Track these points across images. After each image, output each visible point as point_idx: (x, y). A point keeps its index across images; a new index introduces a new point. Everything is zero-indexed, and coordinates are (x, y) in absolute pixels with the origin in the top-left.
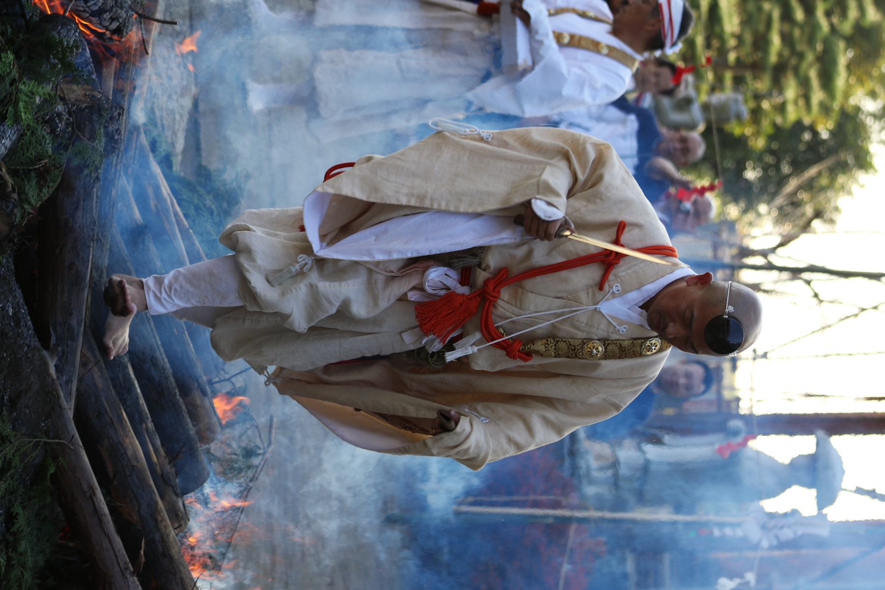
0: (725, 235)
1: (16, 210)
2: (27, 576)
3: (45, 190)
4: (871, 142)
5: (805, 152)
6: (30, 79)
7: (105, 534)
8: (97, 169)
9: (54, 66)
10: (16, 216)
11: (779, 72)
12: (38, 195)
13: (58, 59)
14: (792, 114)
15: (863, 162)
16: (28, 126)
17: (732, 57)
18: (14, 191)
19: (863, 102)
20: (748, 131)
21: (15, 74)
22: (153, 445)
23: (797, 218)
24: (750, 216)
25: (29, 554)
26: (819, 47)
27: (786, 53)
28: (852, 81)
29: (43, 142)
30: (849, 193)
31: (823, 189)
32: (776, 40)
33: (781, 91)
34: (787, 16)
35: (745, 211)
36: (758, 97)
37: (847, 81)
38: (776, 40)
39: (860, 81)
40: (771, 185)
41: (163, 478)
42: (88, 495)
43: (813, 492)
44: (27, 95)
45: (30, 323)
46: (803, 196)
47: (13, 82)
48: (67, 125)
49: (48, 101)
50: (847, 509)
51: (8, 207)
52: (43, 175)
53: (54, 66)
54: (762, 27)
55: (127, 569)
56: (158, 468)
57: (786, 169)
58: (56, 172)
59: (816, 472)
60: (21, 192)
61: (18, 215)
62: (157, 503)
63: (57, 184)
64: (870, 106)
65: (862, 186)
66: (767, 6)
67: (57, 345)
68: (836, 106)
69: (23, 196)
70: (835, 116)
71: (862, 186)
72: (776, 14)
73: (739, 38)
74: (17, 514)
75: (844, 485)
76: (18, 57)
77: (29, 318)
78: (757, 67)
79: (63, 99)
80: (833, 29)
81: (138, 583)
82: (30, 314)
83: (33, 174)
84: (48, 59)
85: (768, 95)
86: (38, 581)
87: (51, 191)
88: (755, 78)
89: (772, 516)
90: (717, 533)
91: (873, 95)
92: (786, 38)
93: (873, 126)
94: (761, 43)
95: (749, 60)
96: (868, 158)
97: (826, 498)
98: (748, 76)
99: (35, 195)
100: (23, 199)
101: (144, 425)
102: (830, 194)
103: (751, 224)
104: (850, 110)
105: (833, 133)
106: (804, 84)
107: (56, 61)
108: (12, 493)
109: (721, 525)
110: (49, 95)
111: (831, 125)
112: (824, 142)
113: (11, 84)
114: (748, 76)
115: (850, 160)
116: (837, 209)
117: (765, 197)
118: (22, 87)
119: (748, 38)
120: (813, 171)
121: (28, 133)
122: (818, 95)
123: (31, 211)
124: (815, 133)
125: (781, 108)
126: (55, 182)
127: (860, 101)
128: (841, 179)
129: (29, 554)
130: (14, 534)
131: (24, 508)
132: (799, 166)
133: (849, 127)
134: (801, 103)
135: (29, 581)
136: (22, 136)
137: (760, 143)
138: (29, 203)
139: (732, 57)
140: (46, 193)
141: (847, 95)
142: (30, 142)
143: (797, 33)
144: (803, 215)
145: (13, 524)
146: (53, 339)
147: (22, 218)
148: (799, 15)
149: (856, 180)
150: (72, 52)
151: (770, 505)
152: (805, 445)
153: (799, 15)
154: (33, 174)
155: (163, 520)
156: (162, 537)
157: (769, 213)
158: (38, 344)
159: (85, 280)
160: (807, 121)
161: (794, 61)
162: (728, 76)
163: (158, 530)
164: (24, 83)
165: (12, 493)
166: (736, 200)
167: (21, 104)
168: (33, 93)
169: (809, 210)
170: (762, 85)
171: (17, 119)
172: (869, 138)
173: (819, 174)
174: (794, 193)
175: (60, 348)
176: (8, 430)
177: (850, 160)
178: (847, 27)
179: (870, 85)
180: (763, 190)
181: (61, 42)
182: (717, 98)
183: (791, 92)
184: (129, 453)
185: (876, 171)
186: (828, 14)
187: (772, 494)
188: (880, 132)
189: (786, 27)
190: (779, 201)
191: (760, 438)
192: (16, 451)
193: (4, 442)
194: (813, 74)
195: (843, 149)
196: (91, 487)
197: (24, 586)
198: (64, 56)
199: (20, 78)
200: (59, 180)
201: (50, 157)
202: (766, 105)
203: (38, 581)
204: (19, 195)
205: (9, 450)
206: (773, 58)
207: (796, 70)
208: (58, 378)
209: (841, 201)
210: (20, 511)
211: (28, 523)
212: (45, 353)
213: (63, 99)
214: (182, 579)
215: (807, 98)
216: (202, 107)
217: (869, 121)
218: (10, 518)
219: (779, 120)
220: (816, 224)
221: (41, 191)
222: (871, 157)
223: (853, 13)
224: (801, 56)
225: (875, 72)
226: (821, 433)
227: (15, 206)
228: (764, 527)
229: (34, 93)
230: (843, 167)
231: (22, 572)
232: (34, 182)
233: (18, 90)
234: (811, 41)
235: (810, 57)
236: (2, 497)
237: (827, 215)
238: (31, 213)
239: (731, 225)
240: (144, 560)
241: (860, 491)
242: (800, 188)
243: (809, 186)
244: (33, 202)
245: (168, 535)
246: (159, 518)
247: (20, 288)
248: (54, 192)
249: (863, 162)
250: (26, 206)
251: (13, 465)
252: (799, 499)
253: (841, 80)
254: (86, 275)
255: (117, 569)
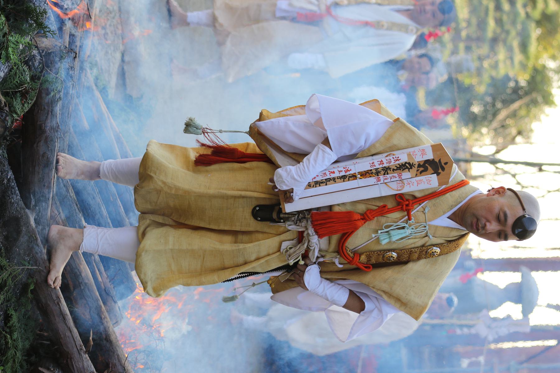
0: (461, 146)
1: (7, 118)
2: (19, 354)
3: (26, 105)
4: (553, 88)
5: (510, 94)
6: (16, 33)
7: (67, 327)
8: (60, 92)
9: (31, 25)
10: (7, 121)
11: (495, 40)
12: (22, 108)
13: (34, 21)
14: (502, 71)
15: (548, 100)
16: (15, 63)
17: (464, 34)
18: (6, 106)
19: (547, 62)
20: (474, 81)
21: (6, 29)
22: (99, 270)
23: (505, 136)
24: (476, 135)
25: (20, 340)
26: (519, 27)
27: (498, 31)
28: (541, 48)
29: (24, 73)
30: (539, 120)
31: (522, 117)
32: (491, 24)
33: (496, 54)
34: (498, 8)
35: (473, 131)
36: (480, 59)
37: (537, 49)
38: (491, 24)
39: (545, 49)
40: (488, 116)
41: (105, 291)
42: (56, 302)
43: (520, 306)
44: (14, 44)
45: (18, 192)
46: (510, 122)
47: (5, 35)
48: (40, 63)
49: (29, 46)
50: (541, 317)
51: (2, 116)
52: (24, 95)
53: (31, 25)
54: (482, 14)
55: (81, 349)
56: (102, 285)
57: (499, 105)
58: (33, 93)
59: (522, 294)
60: (11, 106)
61: (10, 121)
62: (101, 307)
63: (33, 102)
64: (552, 64)
65: (547, 116)
66: (485, 2)
67: (35, 206)
68: (530, 64)
69: (12, 109)
70: (530, 70)
71: (547, 116)
72: (492, 6)
73: (469, 22)
74: (12, 314)
75: (539, 302)
76: (8, 19)
77: (17, 188)
78: (479, 39)
79: (37, 47)
80: (528, 16)
81: (88, 358)
82: (18, 186)
83: (18, 94)
84: (27, 21)
85: (488, 57)
86: (26, 358)
87: (30, 106)
88: (478, 47)
89: (495, 319)
90: (459, 332)
91: (554, 58)
92: (499, 22)
93: (554, 77)
94: (482, 25)
95: (474, 36)
96: (551, 98)
97: (526, 311)
98: (474, 45)
99: (21, 108)
100: (12, 111)
101: (93, 257)
102: (526, 120)
103: (477, 140)
104: (539, 68)
105: (529, 83)
106: (510, 49)
107: (33, 22)
108: (8, 301)
109: (461, 326)
110: (28, 43)
111: (527, 76)
112: (522, 88)
113: (4, 36)
114: (474, 45)
115: (540, 99)
116: (531, 131)
117: (486, 123)
118: (10, 38)
119: (474, 21)
120: (516, 105)
121: (15, 68)
122: (518, 57)
123: (18, 118)
124: (517, 82)
125: (495, 66)
126: (32, 100)
127: (545, 61)
128: (534, 110)
129: (20, 340)
130: (10, 328)
131: (16, 311)
132: (507, 103)
133: (539, 78)
134: (508, 62)
135: (20, 358)
136: (10, 71)
137: (482, 89)
138: (16, 113)
139: (464, 34)
140: (27, 107)
141: (537, 58)
142: (16, 73)
143: (505, 18)
144: (510, 134)
145: (9, 321)
146: (33, 203)
147: (12, 123)
148: (506, 7)
149: (544, 112)
150: (42, 16)
151: (493, 314)
152: (515, 277)
153: (506, 7)
154: (18, 94)
155: (105, 318)
156: (105, 328)
157: (488, 133)
158: (23, 205)
159: (53, 163)
160: (511, 74)
161: (503, 36)
162: (462, 46)
163: (103, 324)
164: (12, 36)
165: (8, 301)
166: (466, 125)
167: (10, 49)
168: (18, 43)
169: (514, 131)
170: (484, 50)
171: (8, 58)
172: (551, 85)
173: (520, 107)
174: (505, 120)
175: (37, 208)
176: (4, 262)
177: (540, 99)
178: (536, 14)
179: (551, 51)
180: (484, 118)
181: (35, 9)
182: (454, 59)
183: (502, 55)
184: (83, 275)
185: (556, 106)
186: (525, 6)
187: (494, 307)
188: (558, 81)
189: (498, 14)
190: (495, 124)
191: (487, 273)
192: (9, 275)
193: (2, 269)
194: (515, 44)
195: (533, 92)
196: (58, 297)
197: (17, 361)
198: (37, 19)
199: (10, 32)
200: (35, 99)
201: (29, 83)
202: (486, 64)
203: (26, 358)
204: (10, 108)
205: (5, 275)
206: (490, 34)
207: (505, 41)
208: (36, 227)
209: (534, 125)
210: (13, 312)
211: (19, 321)
212: (27, 210)
213: (37, 47)
214: (118, 356)
215: (511, 59)
216: (127, 58)
217: (551, 74)
218: (7, 318)
219: (494, 73)
220: (519, 139)
221: (23, 105)
222: (553, 97)
223: (540, 5)
224: (508, 32)
225: (555, 43)
226: (524, 269)
227: (7, 116)
228: (489, 327)
229: (18, 42)
230: (535, 102)
231: (15, 352)
232: (19, 99)
233: (8, 40)
234: (514, 23)
235: (513, 33)
236: (2, 304)
237: (524, 134)
238: (18, 120)
239: (464, 141)
240: (92, 343)
241: (549, 306)
242: (508, 117)
243: (514, 115)
244: (19, 112)
245: (109, 327)
246: (103, 317)
247: (11, 169)
248: (31, 107)
249: (548, 100)
250: (14, 115)
251: (8, 284)
252: (511, 310)
253: (533, 47)
254: (53, 161)
255: (75, 349)
